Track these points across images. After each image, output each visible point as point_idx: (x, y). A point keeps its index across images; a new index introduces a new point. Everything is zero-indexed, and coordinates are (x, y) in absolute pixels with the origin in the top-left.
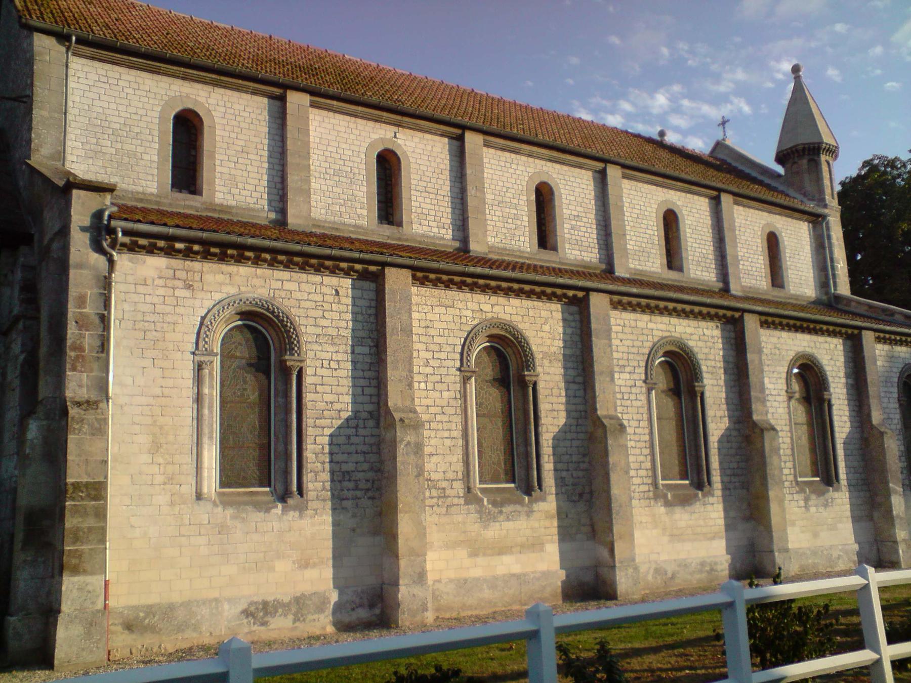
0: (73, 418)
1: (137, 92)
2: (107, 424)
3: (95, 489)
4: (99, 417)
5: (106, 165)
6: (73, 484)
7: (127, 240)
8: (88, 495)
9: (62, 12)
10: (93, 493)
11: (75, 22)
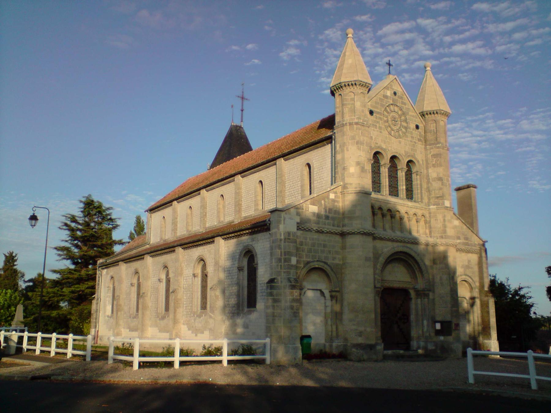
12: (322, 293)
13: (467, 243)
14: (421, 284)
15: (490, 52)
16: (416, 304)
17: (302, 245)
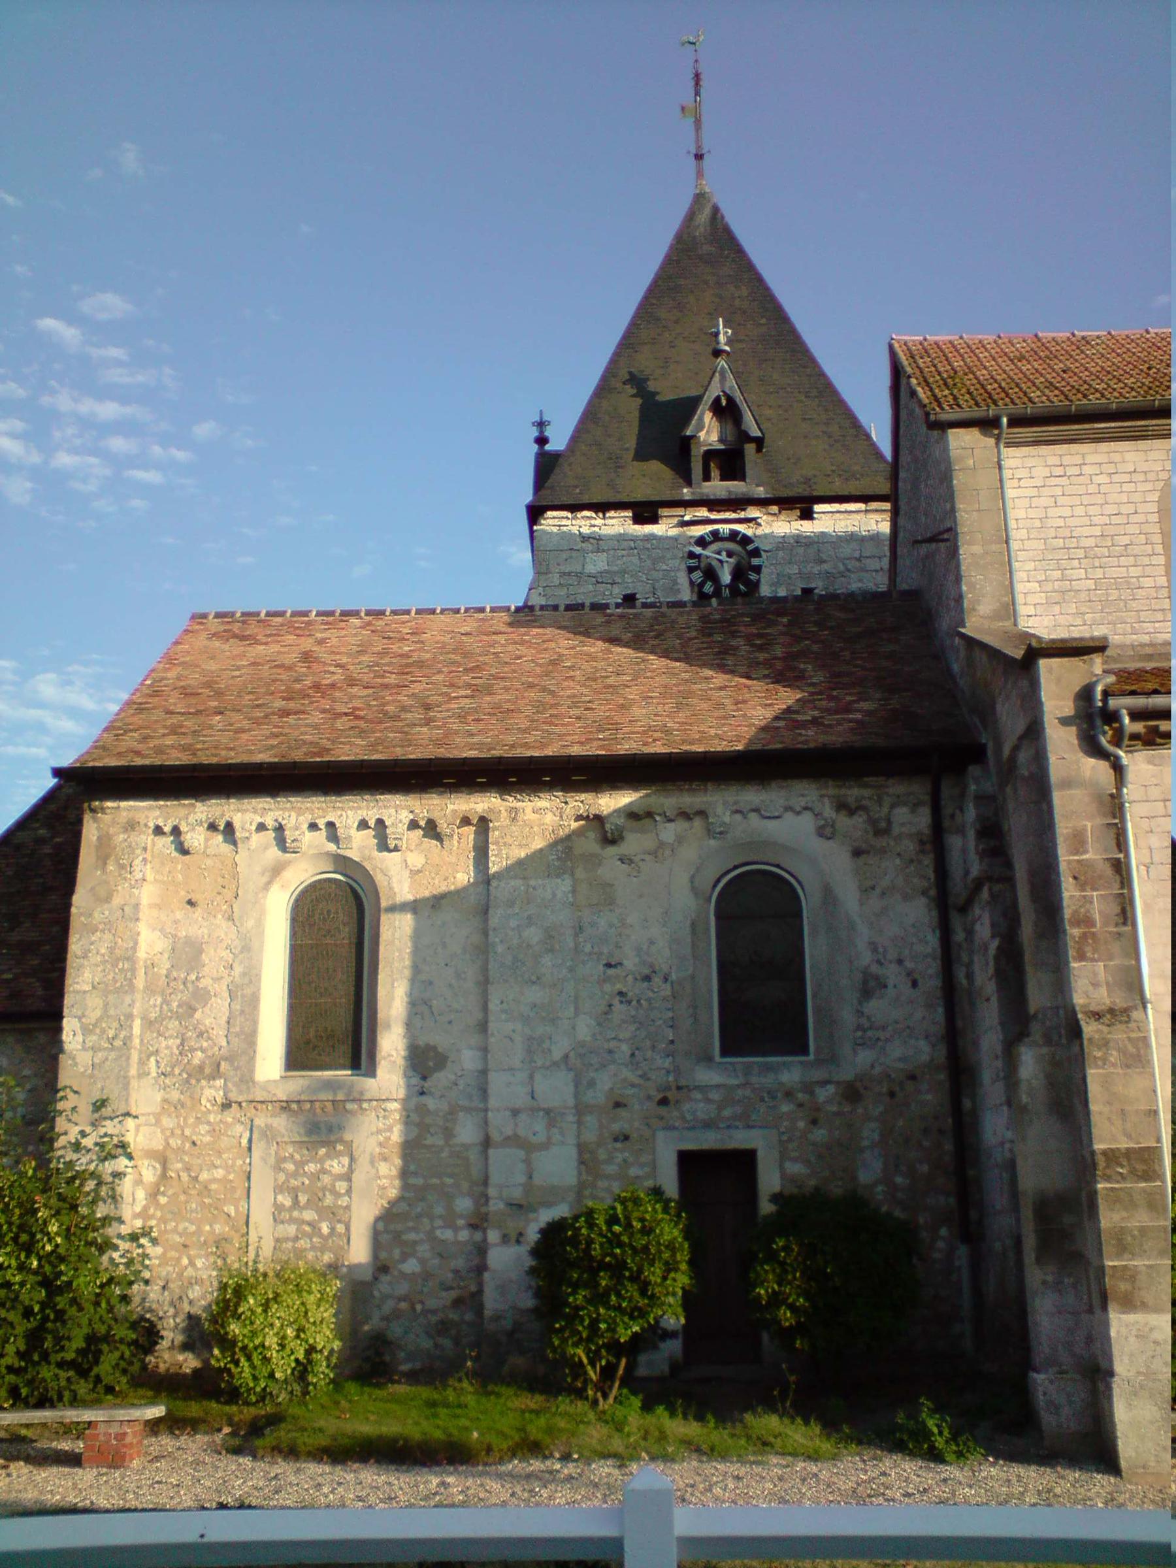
0: (1090, 1040)
1: (1116, 478)
2: (1148, 1045)
3: (1145, 1161)
4: (1134, 1035)
5: (1083, 609)
6: (1105, 1153)
7: (1139, 727)
8: (1133, 1172)
9: (983, 386)
10: (1140, 1167)
11: (1003, 395)
15: (36, 458)
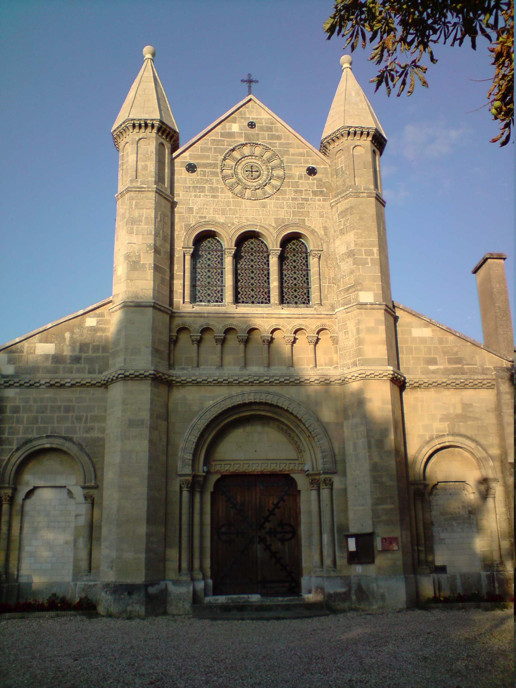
12: (70, 493)
13: (462, 369)
14: (313, 460)
16: (308, 501)
17: (15, 412)
